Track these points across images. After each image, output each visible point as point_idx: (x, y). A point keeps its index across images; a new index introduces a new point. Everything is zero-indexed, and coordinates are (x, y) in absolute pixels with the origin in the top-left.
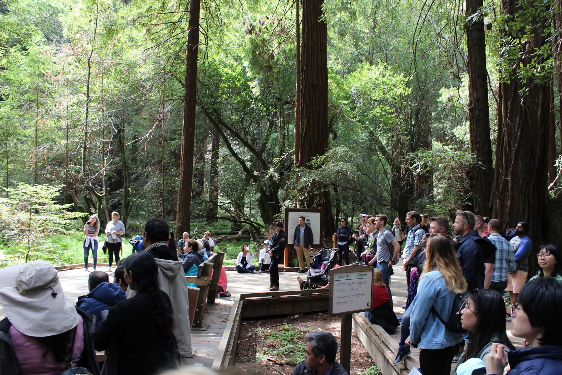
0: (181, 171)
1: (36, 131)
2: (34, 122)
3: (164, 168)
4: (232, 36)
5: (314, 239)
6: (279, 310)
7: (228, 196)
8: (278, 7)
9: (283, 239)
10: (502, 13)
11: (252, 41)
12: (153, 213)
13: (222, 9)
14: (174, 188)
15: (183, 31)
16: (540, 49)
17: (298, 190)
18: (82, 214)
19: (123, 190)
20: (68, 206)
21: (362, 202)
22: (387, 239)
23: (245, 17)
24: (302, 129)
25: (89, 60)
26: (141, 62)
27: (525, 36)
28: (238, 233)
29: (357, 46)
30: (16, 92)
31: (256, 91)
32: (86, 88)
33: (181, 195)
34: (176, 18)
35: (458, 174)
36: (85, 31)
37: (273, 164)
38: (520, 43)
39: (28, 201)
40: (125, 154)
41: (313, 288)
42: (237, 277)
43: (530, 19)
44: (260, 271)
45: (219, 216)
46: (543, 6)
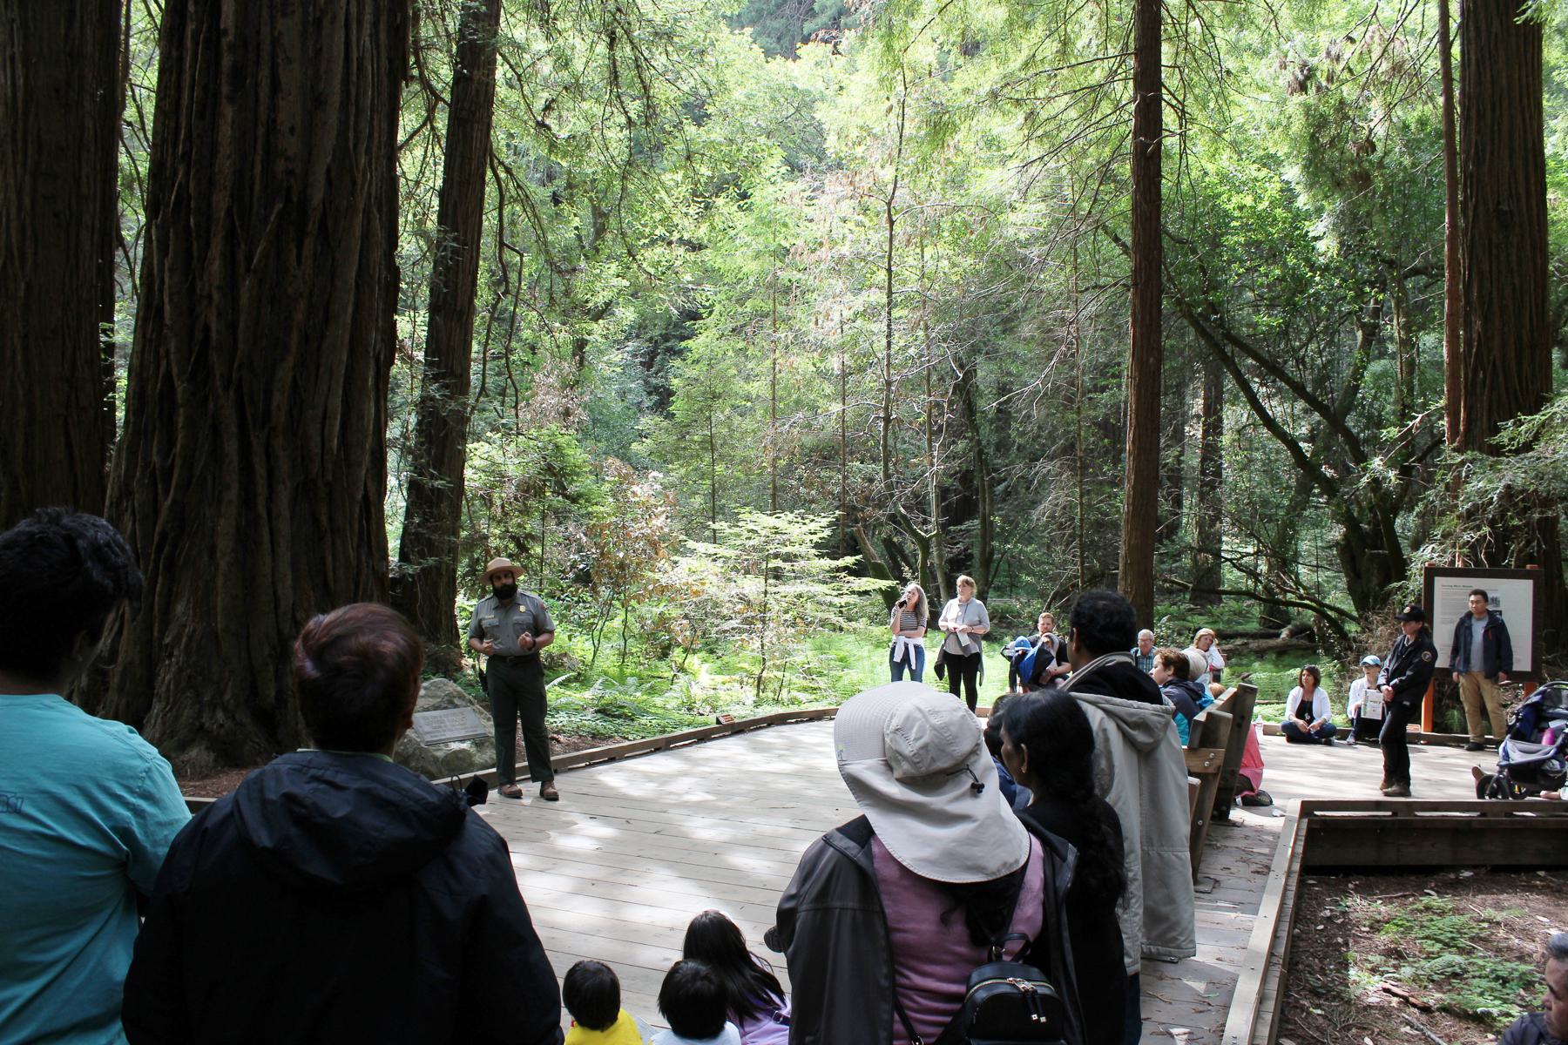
1: (773, 385)
2: (768, 363)
5: (1515, 656)
6: (1411, 853)
11: (1307, 109)
12: (1053, 579)
13: (1219, 33)
15: (1118, 108)
18: (884, 584)
19: (976, 522)
20: (849, 560)
23: (1285, 47)
24: (1468, 343)
25: (889, 204)
26: (1016, 196)
28: (1278, 636)
30: (729, 299)
31: (1327, 247)
32: (882, 276)
33: (1129, 534)
34: (1098, 76)
36: (876, 137)
37: (1382, 446)
39: (762, 550)
40: (982, 431)
41: (1514, 796)
42: (1285, 755)
44: (1351, 739)
45: (1226, 587)
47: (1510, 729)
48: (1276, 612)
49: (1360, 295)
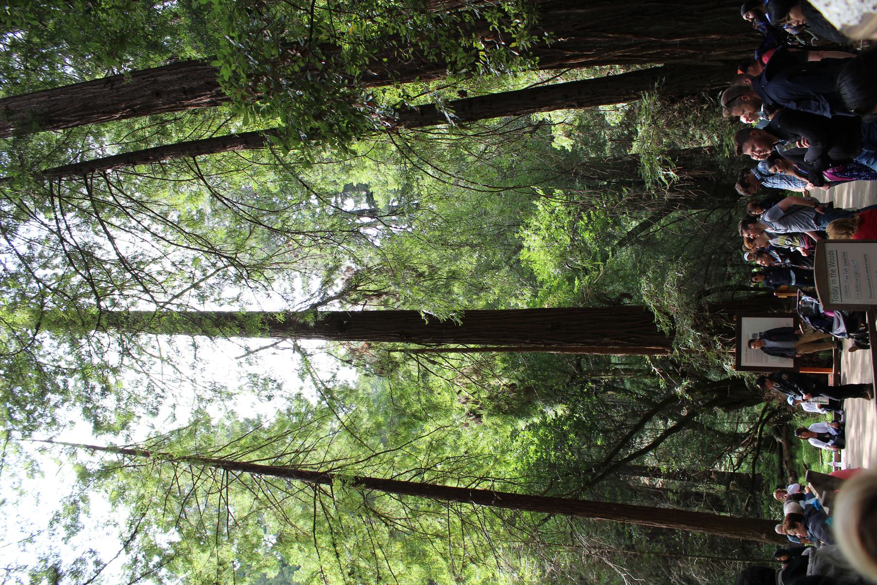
0: (679, 529)
3: (676, 553)
4: (484, 443)
7: (720, 457)
8: (445, 377)
9: (784, 377)
10: (444, 79)
11: (490, 415)
14: (705, 540)
15: (474, 512)
16: (491, 23)
17: (708, 351)
21: (727, 253)
22: (779, 217)
23: (458, 423)
24: (615, 344)
26: (515, 575)
27: (474, 45)
29: (498, 268)
31: (561, 410)
34: (457, 520)
35: (674, 116)
38: (484, 50)
41: (866, 330)
43: (453, 41)
44: (840, 412)
46: (436, 28)
47: (826, 332)
48: (766, 443)
49: (588, 394)
